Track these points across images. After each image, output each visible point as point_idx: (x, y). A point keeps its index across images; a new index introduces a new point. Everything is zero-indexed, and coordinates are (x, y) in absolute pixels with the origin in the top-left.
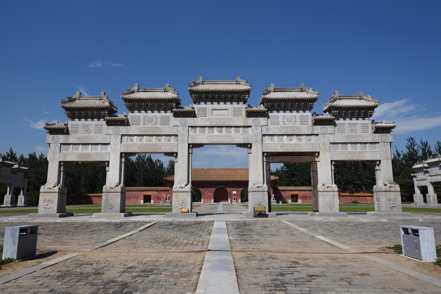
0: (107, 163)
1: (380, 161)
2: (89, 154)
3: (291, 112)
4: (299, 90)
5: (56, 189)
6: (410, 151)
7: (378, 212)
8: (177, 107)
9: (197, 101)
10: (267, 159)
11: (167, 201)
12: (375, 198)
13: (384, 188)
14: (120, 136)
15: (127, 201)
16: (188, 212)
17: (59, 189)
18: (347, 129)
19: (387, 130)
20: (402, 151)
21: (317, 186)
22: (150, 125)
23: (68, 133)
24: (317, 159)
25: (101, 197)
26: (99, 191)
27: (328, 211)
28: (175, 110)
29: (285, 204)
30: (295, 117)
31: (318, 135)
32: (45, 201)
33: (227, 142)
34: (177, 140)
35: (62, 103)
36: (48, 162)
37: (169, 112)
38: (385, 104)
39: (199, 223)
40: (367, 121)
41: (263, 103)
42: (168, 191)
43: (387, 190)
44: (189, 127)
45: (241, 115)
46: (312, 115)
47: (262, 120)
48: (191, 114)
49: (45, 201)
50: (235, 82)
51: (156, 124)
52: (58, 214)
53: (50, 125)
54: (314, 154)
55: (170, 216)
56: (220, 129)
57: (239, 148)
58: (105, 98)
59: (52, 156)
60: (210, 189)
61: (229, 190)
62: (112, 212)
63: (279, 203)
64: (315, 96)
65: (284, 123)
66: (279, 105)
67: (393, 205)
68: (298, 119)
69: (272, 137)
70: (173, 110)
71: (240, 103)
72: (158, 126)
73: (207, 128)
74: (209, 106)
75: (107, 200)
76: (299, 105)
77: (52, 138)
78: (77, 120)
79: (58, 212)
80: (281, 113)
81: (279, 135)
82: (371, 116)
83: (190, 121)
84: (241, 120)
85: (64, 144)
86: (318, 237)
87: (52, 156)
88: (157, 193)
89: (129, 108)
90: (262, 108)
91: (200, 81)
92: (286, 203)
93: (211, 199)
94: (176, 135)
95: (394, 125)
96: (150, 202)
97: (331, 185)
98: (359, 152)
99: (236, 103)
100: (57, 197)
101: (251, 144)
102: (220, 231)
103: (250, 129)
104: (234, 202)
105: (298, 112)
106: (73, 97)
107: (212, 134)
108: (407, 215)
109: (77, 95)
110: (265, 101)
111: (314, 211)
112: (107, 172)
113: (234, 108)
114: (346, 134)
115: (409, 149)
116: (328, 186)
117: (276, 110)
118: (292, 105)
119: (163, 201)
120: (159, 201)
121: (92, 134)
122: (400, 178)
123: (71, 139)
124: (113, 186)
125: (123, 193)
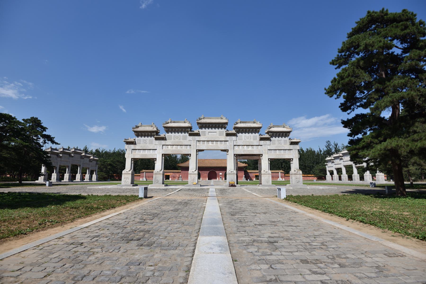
0: (155, 159)
1: (293, 159)
2: (146, 154)
3: (249, 134)
4: (253, 122)
5: (130, 172)
6: (327, 149)
7: (292, 185)
8: (191, 131)
9: (201, 128)
10: (236, 158)
11: (180, 179)
12: (290, 177)
13: (294, 172)
14: (162, 145)
15: (144, 180)
16: (196, 184)
17: (132, 172)
18: (277, 142)
19: (296, 143)
20: (323, 149)
21: (261, 171)
22: (177, 140)
23: (135, 144)
24: (261, 158)
25: (289, 176)
26: (138, 173)
27: (266, 184)
28: (190, 132)
29: (252, 181)
30: (250, 136)
31: (262, 145)
32: (125, 178)
33: (216, 149)
34: (191, 148)
35: (133, 129)
36: (126, 158)
37: (186, 133)
38: (315, 117)
39: (203, 189)
40: (287, 139)
41: (234, 129)
42: (180, 172)
43: (296, 173)
44: (197, 141)
45: (223, 135)
46: (259, 135)
47: (234, 138)
48: (198, 135)
49: (125, 178)
50: (220, 118)
51: (180, 139)
52: (132, 185)
53: (126, 140)
54: (260, 155)
55: (187, 186)
56: (212, 142)
57: (222, 152)
58: (154, 126)
59: (128, 156)
60: (206, 172)
61: (217, 172)
62: (158, 184)
63: (247, 180)
64: (260, 126)
65: (245, 140)
66: (242, 130)
67: (298, 181)
68: (252, 137)
69: (239, 146)
70: (189, 132)
71: (223, 129)
72: (181, 140)
73: (206, 142)
74: (207, 130)
75: (156, 178)
76: (252, 130)
77: (128, 147)
78: (140, 137)
79: (131, 184)
80: (244, 134)
81: (242, 145)
82: (288, 136)
83: (197, 138)
84: (224, 138)
85: (134, 149)
86: (253, 194)
87: (128, 156)
88: (173, 174)
89: (166, 131)
90: (234, 132)
91: (202, 117)
92: (252, 180)
93: (206, 178)
94: (190, 145)
95: (300, 141)
96: (169, 179)
97: (268, 171)
98: (283, 154)
99: (220, 129)
100: (131, 176)
101: (228, 150)
102: (212, 191)
103: (228, 142)
104: (221, 180)
105: (252, 134)
106: (138, 126)
107: (208, 145)
108: (305, 186)
109: (140, 125)
110: (235, 128)
111: (260, 184)
112: (155, 164)
113: (220, 131)
114: (276, 145)
115: (327, 147)
116: (266, 171)
117: (241, 133)
118: (249, 130)
119: (177, 179)
120: (175, 179)
121: (148, 144)
122: (320, 165)
123: (137, 147)
124: (158, 171)
125: (132, 174)
